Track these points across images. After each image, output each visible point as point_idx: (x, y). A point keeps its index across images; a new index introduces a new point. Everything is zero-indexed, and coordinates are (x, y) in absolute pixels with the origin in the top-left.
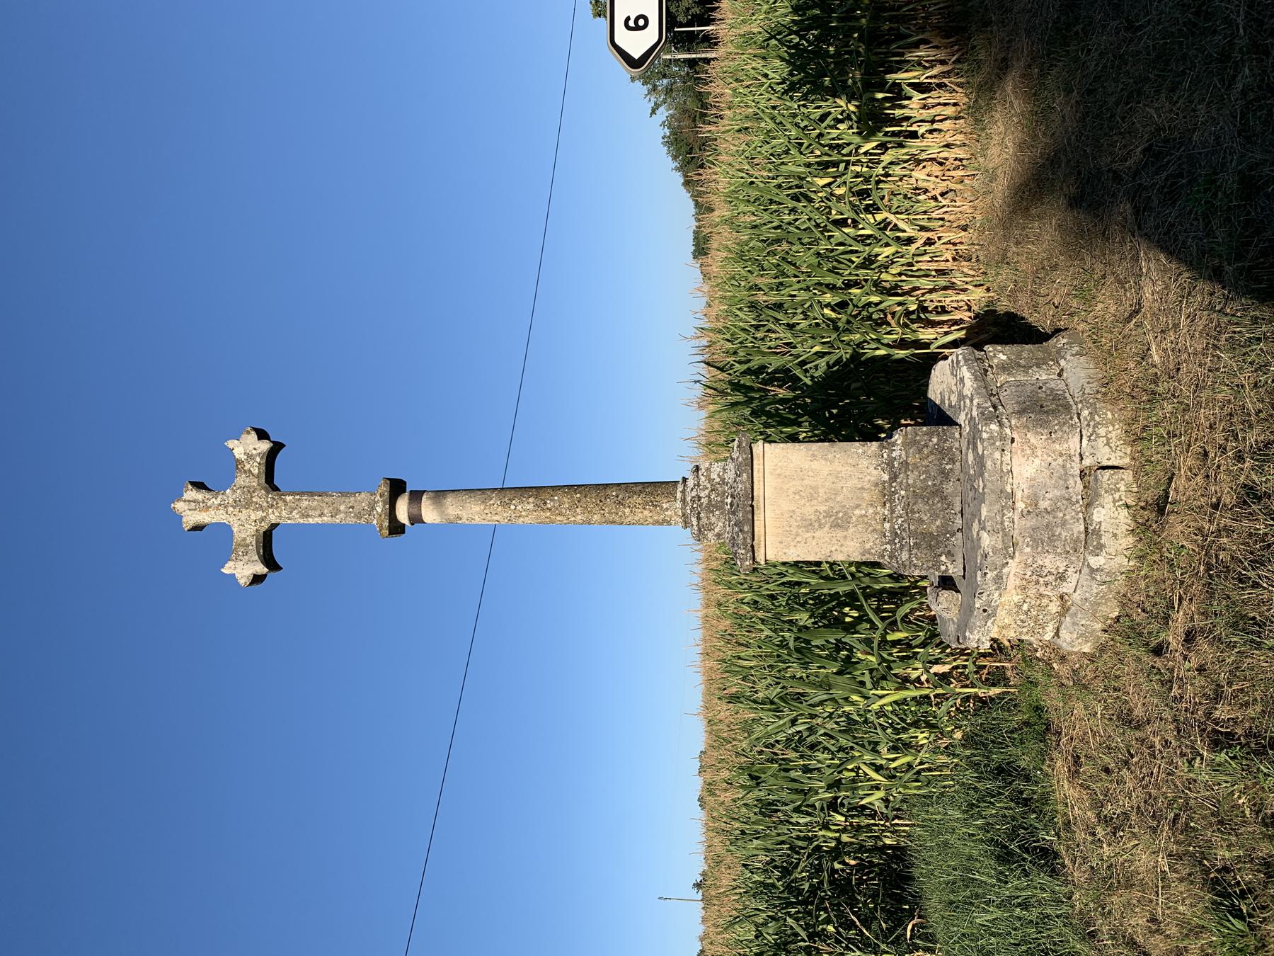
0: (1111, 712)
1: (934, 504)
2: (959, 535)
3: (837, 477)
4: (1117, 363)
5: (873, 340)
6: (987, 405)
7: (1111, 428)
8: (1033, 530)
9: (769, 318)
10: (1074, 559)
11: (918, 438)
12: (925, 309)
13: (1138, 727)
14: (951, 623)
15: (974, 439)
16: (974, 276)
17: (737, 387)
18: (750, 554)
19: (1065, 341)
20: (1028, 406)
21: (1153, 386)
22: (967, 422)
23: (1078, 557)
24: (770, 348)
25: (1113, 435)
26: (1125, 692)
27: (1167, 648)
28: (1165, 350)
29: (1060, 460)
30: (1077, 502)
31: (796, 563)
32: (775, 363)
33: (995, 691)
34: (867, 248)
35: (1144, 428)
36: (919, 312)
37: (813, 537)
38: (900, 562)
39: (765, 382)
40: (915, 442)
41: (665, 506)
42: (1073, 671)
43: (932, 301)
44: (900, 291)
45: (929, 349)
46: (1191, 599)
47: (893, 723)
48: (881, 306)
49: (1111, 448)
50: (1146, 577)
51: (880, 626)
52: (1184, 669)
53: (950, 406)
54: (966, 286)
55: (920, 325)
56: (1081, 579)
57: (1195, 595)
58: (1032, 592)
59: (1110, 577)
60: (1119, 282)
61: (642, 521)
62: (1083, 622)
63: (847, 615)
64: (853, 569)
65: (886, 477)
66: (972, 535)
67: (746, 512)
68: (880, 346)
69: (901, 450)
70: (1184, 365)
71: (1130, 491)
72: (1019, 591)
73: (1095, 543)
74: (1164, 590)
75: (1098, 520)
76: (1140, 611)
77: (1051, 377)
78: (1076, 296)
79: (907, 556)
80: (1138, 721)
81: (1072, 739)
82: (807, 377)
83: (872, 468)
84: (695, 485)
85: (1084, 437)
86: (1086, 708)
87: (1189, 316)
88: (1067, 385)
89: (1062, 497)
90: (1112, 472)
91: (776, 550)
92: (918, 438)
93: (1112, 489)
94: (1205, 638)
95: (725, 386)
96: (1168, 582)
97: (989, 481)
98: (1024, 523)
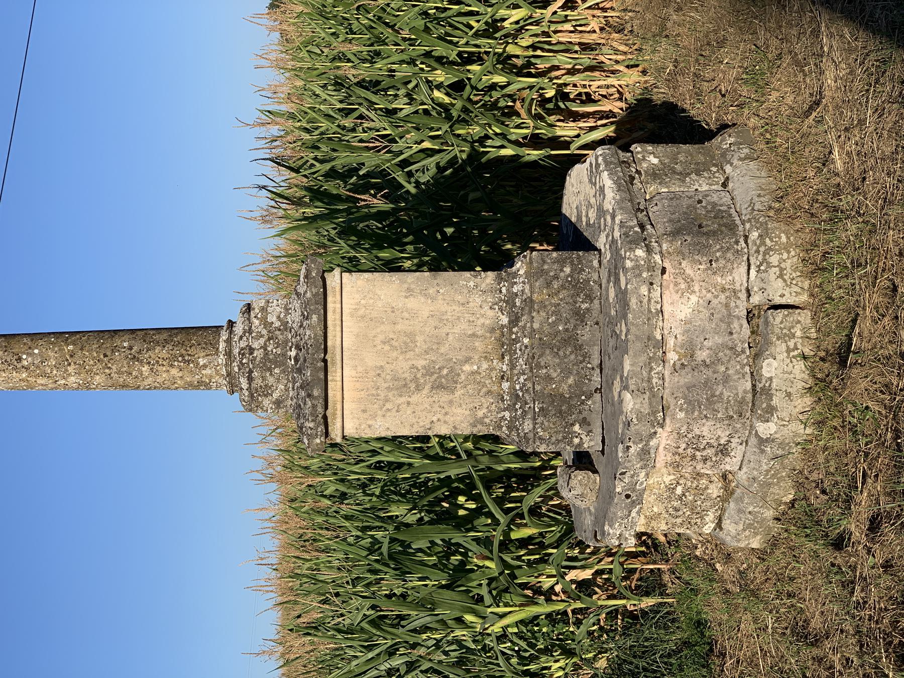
0: (784, 625)
1: (565, 356)
2: (597, 396)
3: (441, 320)
4: (793, 170)
5: (496, 134)
6: (632, 224)
7: (785, 256)
8: (688, 388)
9: (361, 101)
10: (738, 426)
11: (546, 267)
12: (565, 97)
13: (815, 643)
14: (587, 514)
15: (616, 268)
16: (625, 53)
17: (317, 194)
18: (321, 428)
19: (732, 140)
20: (683, 225)
21: (835, 200)
22: (608, 246)
23: (744, 424)
24: (361, 141)
25: (788, 264)
26: (801, 599)
27: (849, 539)
28: (849, 154)
29: (722, 297)
30: (743, 352)
31: (394, 438)
32: (370, 161)
33: (648, 602)
34: (489, 9)
35: (825, 255)
36: (557, 100)
37: (409, 403)
38: (522, 434)
39: (356, 189)
40: (542, 272)
41: (202, 362)
42: (740, 572)
43: (575, 86)
44: (533, 71)
45: (569, 149)
46: (877, 476)
47: (519, 650)
48: (507, 91)
49: (785, 281)
50: (825, 449)
51: (502, 521)
52: (868, 565)
53: (588, 224)
54: (617, 67)
55: (559, 117)
56: (748, 454)
57: (881, 471)
58: (687, 470)
59: (783, 449)
60: (797, 63)
61: (168, 383)
62: (751, 509)
63: (461, 507)
64: (469, 445)
65: (505, 320)
66: (613, 397)
67: (315, 370)
68: (506, 143)
69: (524, 283)
70: (871, 173)
71: (808, 337)
72: (670, 469)
73: (764, 405)
74: (847, 465)
75: (768, 375)
76: (818, 492)
77: (713, 187)
78: (746, 82)
79: (531, 426)
80: (816, 635)
81: (738, 662)
82: (410, 183)
83: (486, 308)
84: (244, 333)
85: (752, 267)
86: (755, 620)
87: (877, 110)
88: (733, 199)
89: (724, 346)
90: (786, 313)
91: (357, 422)
92: (546, 267)
93: (785, 335)
94: (892, 525)
95: (300, 193)
96: (852, 455)
97: (633, 324)
98: (676, 379)
